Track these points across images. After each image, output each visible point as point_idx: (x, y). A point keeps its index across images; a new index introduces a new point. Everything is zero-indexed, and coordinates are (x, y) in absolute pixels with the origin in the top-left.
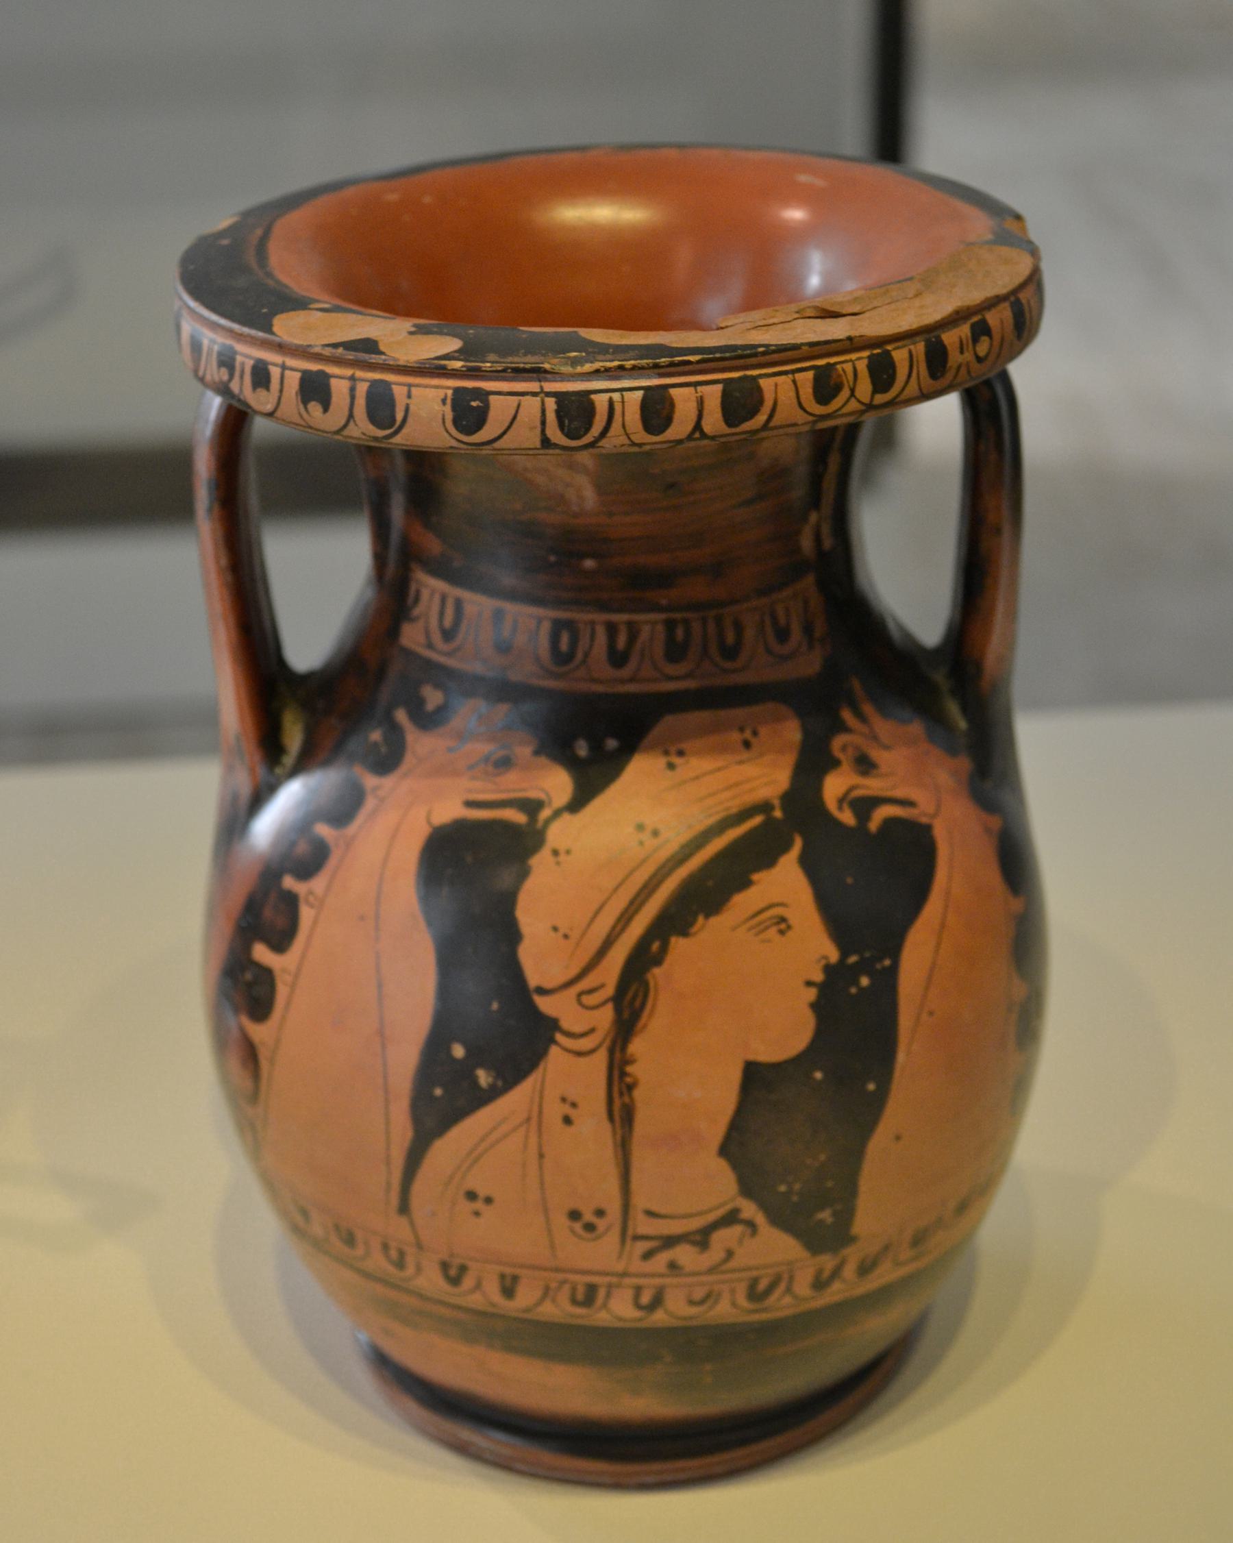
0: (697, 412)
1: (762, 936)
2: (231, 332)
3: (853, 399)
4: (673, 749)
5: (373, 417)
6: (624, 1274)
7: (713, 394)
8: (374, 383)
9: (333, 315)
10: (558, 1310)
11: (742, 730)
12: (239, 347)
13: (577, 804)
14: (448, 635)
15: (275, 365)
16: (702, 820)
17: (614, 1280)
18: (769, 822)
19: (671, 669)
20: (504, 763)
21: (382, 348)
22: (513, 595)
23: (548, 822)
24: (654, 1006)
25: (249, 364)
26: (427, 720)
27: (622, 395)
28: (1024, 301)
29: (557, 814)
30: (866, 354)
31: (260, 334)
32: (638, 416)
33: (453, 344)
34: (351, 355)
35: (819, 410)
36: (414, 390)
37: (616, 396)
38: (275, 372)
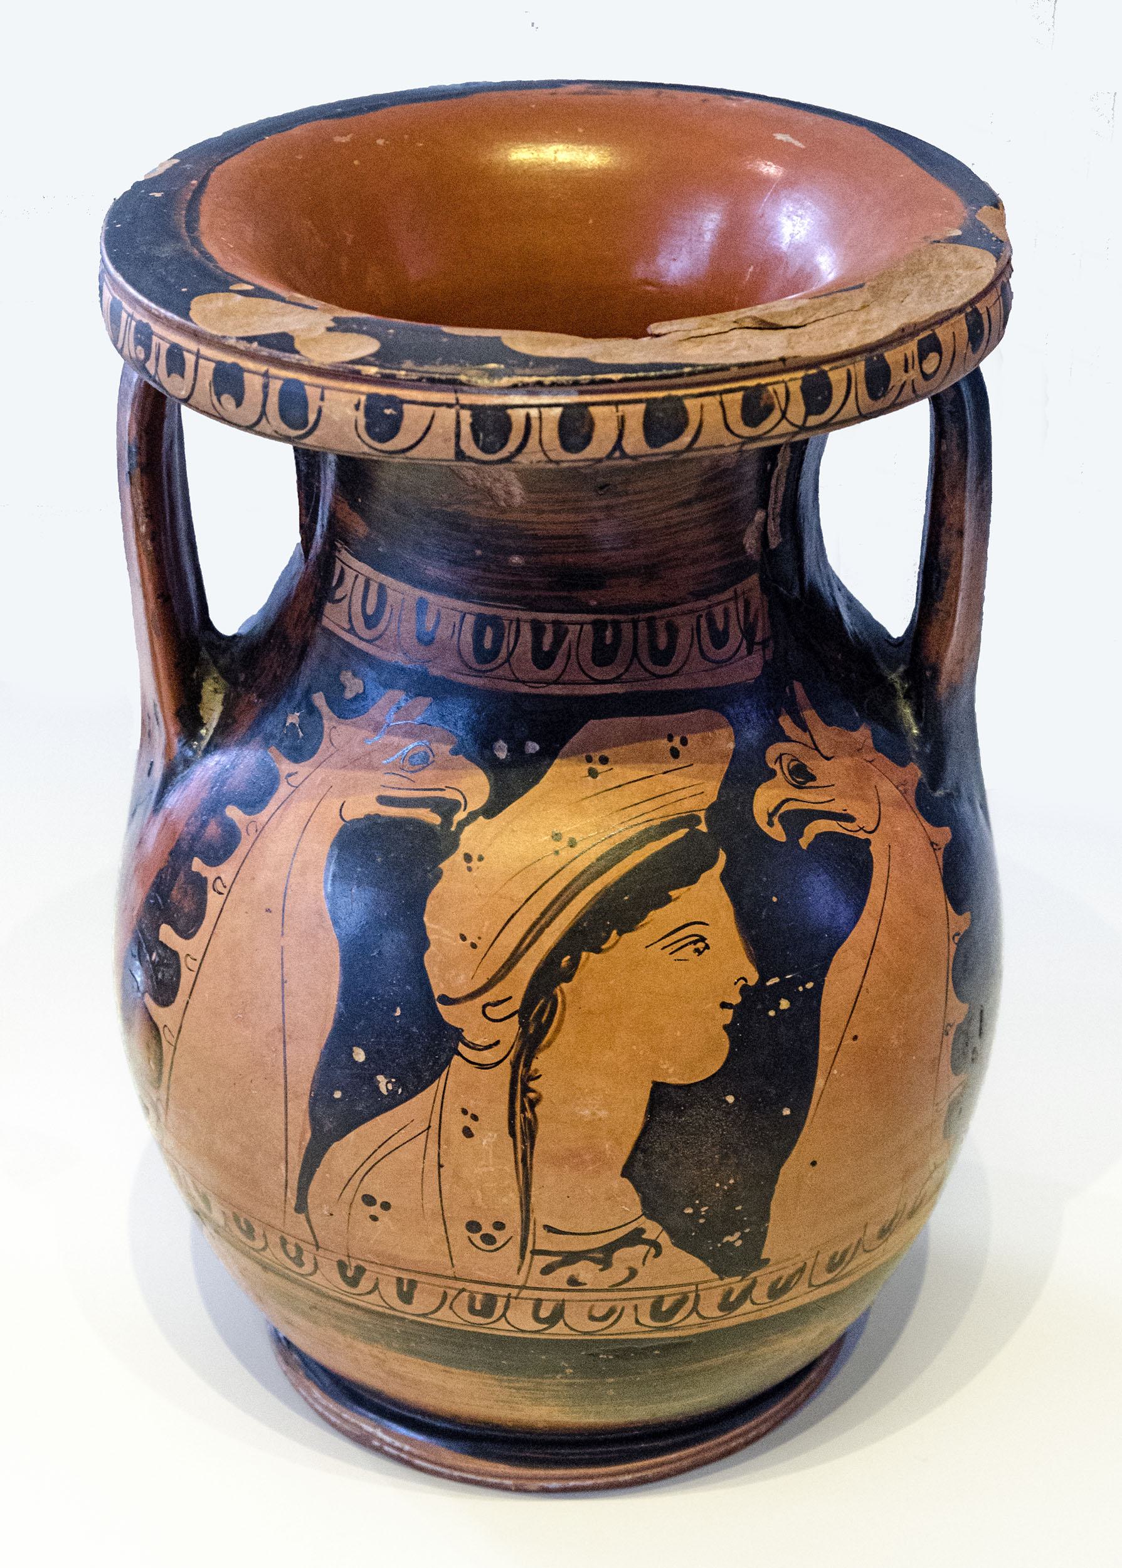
0: (617, 432)
1: (679, 955)
2: (148, 310)
3: (784, 422)
4: (596, 756)
5: (284, 417)
6: (523, 1287)
7: (635, 414)
8: (287, 382)
9: (254, 300)
10: (456, 1317)
11: (670, 738)
12: (156, 328)
13: (491, 810)
14: (371, 621)
15: (189, 351)
16: (622, 830)
17: (514, 1292)
18: (693, 835)
19: (597, 673)
20: (425, 761)
21: (297, 346)
22: (436, 587)
23: (462, 825)
24: (561, 1022)
25: (165, 347)
26: (345, 709)
27: (540, 412)
28: (983, 311)
29: (472, 817)
30: (800, 374)
31: (177, 318)
32: (555, 434)
33: (370, 346)
34: (265, 352)
35: (747, 431)
36: (327, 393)
37: (534, 412)
38: (190, 359)
